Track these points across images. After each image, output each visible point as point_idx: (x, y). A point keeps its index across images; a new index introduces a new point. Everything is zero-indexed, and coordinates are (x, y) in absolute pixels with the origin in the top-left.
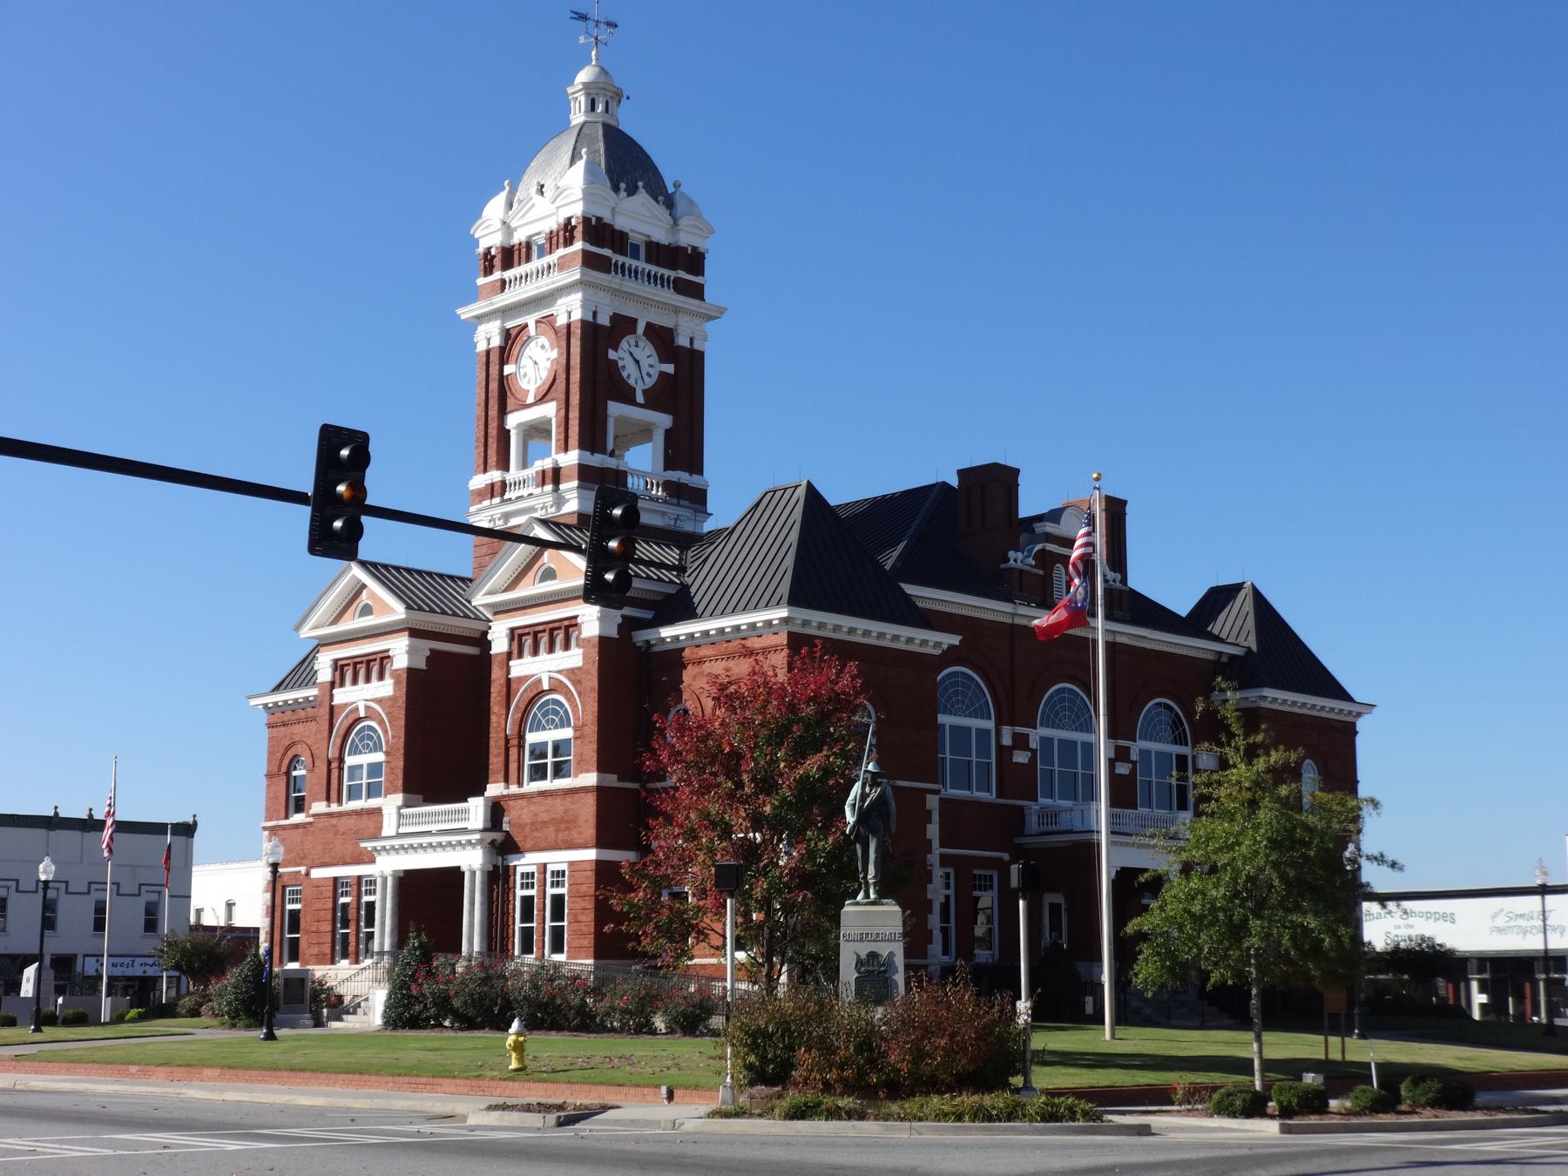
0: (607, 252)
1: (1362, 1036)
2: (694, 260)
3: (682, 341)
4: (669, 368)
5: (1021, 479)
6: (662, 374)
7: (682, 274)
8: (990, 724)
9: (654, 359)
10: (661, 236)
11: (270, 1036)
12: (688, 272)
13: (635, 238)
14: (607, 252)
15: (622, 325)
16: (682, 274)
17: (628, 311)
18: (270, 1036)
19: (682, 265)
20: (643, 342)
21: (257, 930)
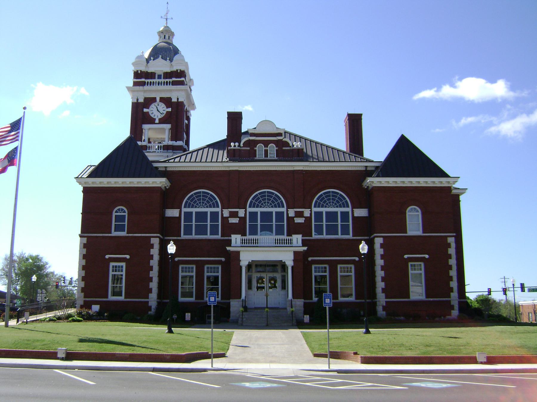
0: (143, 80)
1: (376, 299)
2: (181, 74)
3: (174, 100)
4: (170, 110)
5: (363, 117)
6: (148, 108)
7: (174, 79)
8: (349, 210)
9: (165, 108)
10: (168, 70)
11: (368, 332)
12: (176, 78)
13: (158, 73)
14: (143, 80)
15: (149, 101)
16: (174, 79)
17: (152, 95)
18: (368, 332)
19: (178, 77)
20: (161, 104)
21: (304, 303)
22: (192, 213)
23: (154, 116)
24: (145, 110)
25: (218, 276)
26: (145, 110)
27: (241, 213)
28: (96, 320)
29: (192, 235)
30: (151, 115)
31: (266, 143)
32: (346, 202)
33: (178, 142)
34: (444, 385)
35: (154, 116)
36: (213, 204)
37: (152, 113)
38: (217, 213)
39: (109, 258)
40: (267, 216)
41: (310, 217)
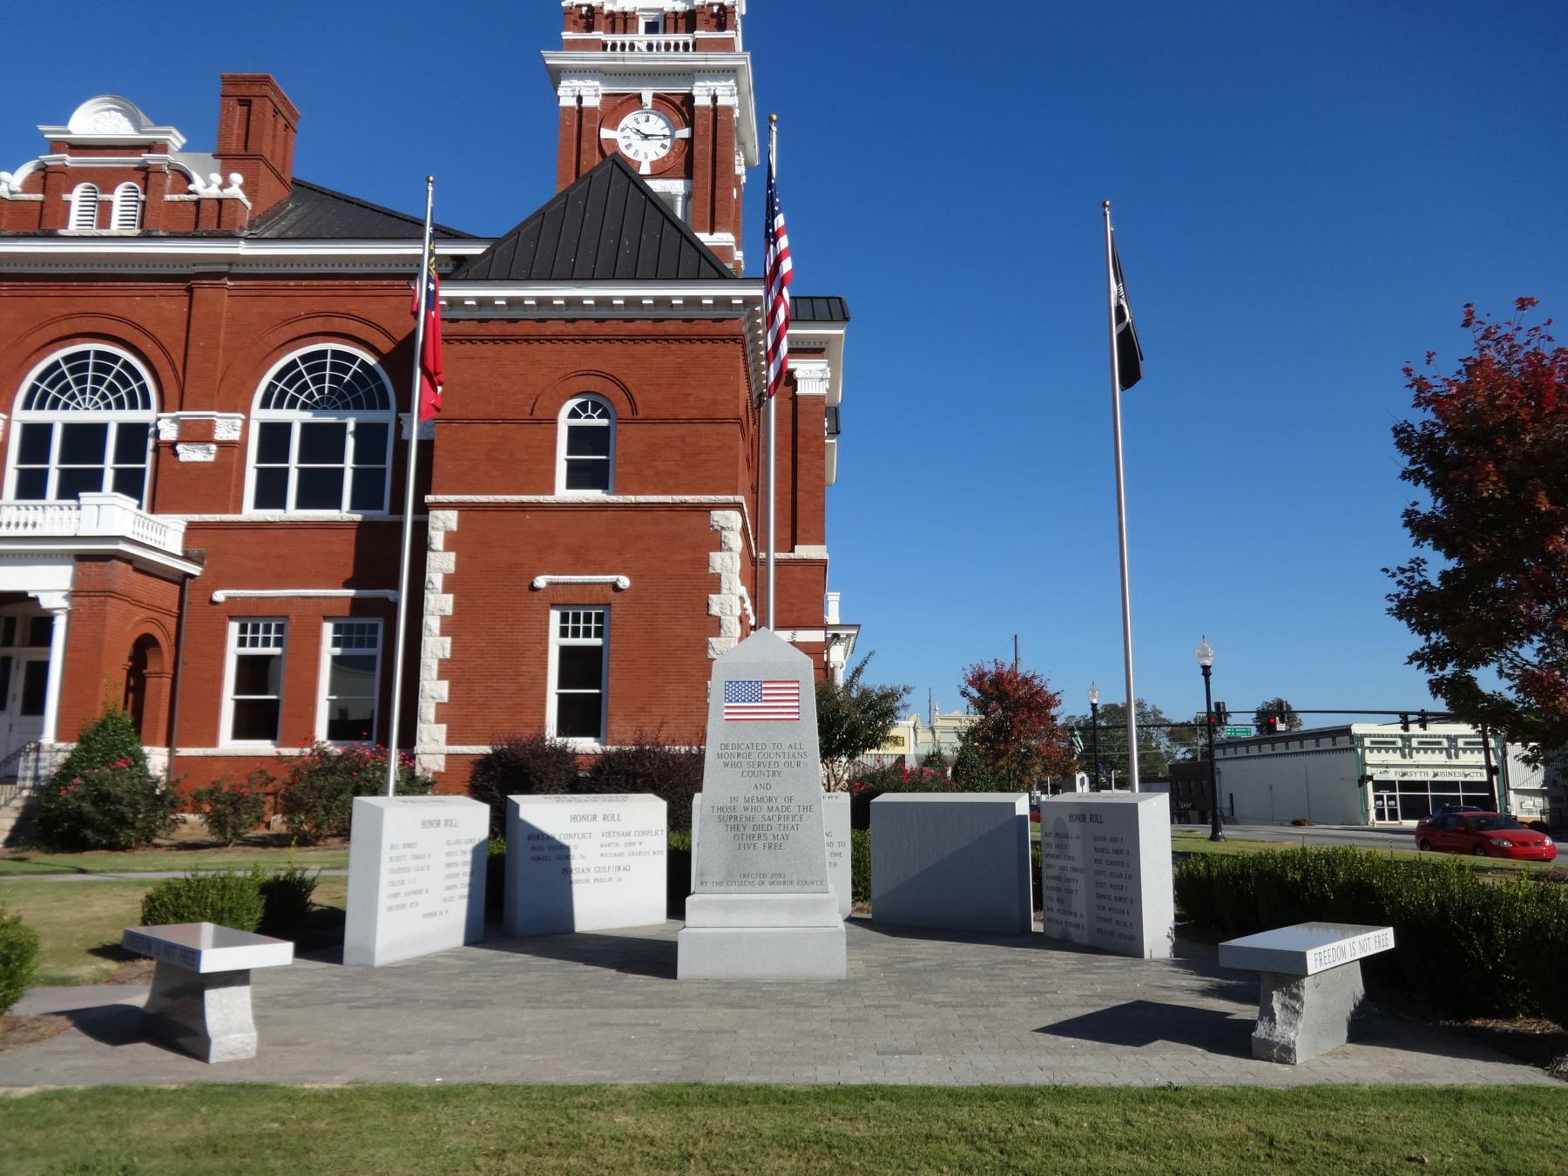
22: (103, 428)
23: (636, 153)
24: (605, 133)
25: (374, 658)
26: (605, 133)
27: (227, 427)
28: (590, 791)
29: (338, 506)
30: (624, 151)
31: (106, 180)
32: (382, 388)
33: (716, 235)
34: (783, 919)
35: (636, 153)
36: (132, 395)
37: (628, 146)
38: (383, 427)
39: (229, 598)
40: (84, 441)
41: (242, 445)
